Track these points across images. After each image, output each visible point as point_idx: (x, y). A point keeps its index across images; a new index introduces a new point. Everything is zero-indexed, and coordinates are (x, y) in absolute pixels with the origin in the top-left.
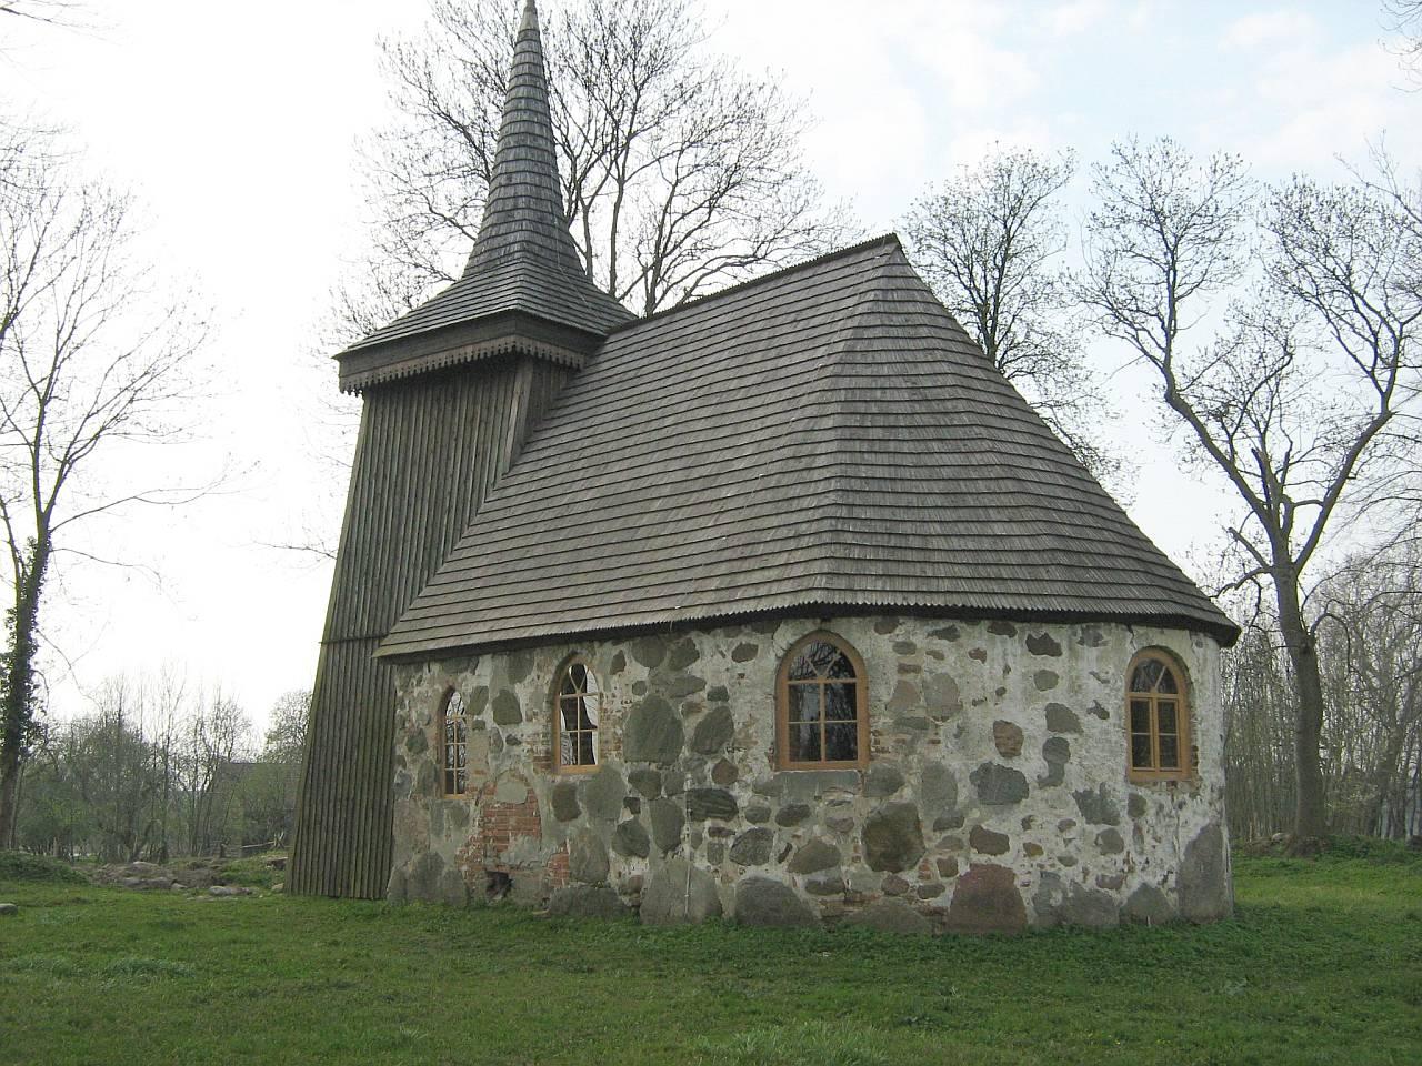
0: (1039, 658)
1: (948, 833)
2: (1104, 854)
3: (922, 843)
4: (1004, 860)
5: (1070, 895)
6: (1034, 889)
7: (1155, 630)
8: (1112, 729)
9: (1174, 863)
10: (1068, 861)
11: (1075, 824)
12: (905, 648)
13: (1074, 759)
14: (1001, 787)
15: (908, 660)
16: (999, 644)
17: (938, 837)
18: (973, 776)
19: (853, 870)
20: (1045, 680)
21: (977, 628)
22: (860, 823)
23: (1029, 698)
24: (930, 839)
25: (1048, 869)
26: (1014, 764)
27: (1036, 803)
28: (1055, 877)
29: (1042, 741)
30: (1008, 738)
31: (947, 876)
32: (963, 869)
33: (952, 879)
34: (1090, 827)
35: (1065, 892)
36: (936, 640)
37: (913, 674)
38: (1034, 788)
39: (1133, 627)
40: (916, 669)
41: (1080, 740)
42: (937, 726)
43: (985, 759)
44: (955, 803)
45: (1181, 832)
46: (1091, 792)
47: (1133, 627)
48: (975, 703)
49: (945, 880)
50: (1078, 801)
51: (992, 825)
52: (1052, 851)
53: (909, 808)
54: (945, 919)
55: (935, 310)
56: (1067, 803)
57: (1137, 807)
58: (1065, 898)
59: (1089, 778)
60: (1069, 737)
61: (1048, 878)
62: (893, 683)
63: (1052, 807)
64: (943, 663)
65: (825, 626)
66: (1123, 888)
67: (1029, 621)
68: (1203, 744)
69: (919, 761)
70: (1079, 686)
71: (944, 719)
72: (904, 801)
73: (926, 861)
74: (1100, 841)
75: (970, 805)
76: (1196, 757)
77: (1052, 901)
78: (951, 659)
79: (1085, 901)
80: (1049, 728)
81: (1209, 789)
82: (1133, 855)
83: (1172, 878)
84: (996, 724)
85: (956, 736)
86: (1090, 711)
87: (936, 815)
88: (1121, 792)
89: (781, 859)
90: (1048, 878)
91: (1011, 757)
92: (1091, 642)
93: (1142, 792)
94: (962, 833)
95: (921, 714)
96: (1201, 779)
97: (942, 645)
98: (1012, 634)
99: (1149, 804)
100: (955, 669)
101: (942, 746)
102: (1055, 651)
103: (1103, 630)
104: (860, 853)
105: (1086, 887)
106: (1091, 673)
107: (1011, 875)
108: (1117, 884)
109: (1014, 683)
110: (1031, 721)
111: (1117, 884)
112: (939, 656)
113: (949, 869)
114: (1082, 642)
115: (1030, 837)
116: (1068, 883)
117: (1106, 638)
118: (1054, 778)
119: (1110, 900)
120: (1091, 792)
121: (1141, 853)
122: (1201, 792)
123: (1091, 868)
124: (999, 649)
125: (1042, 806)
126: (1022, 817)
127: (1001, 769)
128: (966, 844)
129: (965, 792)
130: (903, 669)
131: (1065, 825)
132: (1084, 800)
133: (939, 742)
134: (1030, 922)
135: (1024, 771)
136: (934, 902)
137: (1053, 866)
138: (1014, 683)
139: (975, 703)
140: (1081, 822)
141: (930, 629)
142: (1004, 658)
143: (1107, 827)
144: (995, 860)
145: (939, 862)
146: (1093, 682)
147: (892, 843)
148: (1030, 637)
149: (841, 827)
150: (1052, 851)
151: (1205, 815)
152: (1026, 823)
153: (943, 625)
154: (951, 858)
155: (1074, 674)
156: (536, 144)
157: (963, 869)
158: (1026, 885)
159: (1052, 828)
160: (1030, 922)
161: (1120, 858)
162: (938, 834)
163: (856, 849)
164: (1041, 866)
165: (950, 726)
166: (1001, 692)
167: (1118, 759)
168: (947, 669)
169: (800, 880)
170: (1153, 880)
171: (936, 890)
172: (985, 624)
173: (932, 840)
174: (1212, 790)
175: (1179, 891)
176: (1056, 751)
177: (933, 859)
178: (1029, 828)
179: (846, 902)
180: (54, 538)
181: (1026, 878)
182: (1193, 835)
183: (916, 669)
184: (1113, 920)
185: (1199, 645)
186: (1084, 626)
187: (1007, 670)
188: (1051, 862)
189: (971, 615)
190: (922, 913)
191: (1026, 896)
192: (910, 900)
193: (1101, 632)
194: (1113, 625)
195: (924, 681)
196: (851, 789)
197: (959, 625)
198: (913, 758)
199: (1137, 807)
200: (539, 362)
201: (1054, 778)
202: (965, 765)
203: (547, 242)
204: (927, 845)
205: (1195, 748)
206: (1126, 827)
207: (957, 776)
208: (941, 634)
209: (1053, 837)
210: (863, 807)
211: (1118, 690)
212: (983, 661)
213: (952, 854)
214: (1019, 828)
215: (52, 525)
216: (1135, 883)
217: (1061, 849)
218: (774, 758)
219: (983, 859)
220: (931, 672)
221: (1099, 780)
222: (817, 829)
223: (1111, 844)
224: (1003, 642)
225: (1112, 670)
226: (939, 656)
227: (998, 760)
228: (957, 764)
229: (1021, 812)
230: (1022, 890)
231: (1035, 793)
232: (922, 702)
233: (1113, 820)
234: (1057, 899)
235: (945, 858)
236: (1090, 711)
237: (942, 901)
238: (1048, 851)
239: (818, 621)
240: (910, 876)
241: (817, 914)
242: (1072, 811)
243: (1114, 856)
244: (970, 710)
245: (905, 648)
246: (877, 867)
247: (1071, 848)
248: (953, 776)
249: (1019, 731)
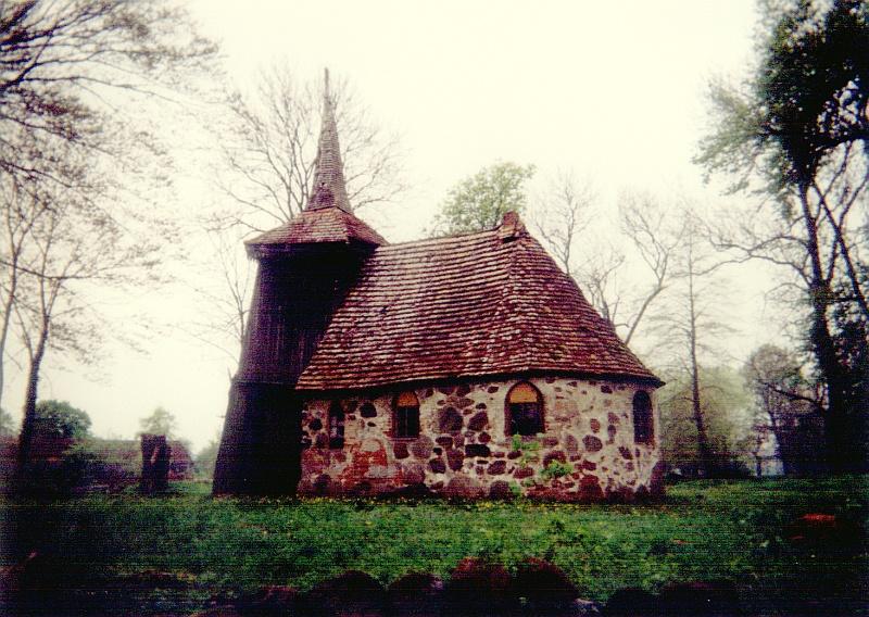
14: (593, 444)
26: (597, 435)
30: (595, 426)
32: (582, 476)
97: (571, 388)
107: (597, 479)
111: (633, 483)
129: (581, 446)
136: (571, 490)
157: (582, 476)
191: (603, 488)
198: (562, 433)
201: (611, 441)
217: (615, 469)
227: (592, 434)
228: (579, 437)
231: (604, 446)
234: (613, 489)
237: (574, 489)
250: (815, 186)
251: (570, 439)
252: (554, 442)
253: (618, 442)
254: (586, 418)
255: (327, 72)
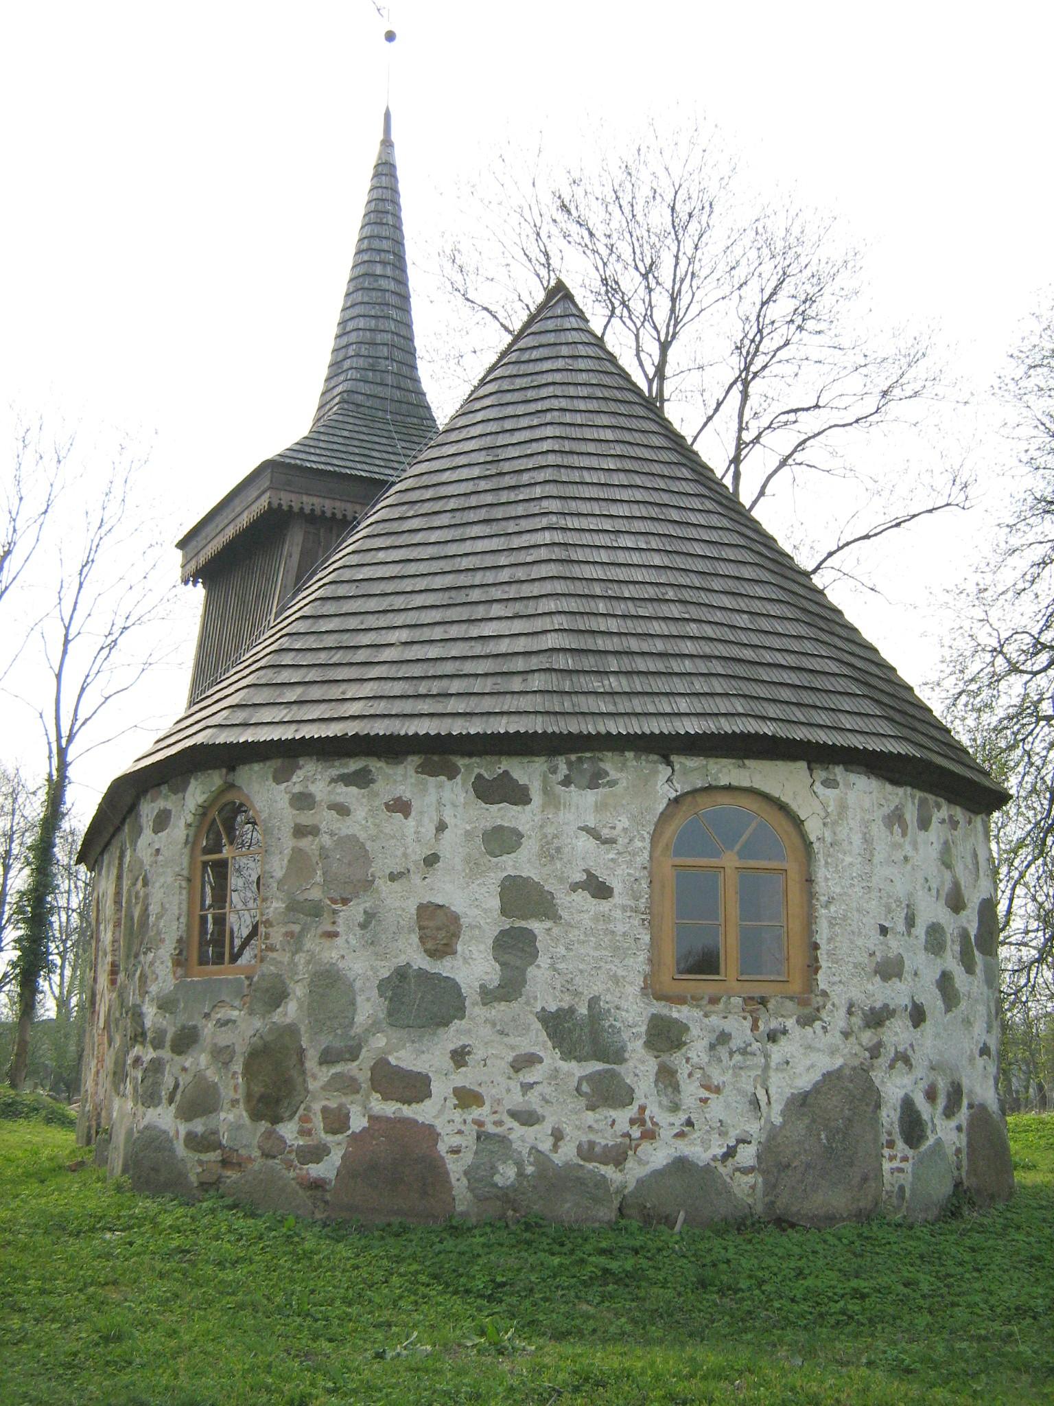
0: (495, 807)
1: (338, 1068)
2: (592, 1107)
3: (305, 1081)
4: (423, 1112)
5: (530, 1169)
6: (468, 1158)
7: (724, 761)
8: (618, 914)
9: (754, 1128)
10: (527, 1118)
11: (541, 1060)
12: (303, 801)
13: (543, 960)
14: (423, 1001)
15: (306, 818)
16: (432, 790)
17: (325, 1074)
18: (383, 985)
19: (231, 1119)
20: (501, 841)
21: (400, 770)
22: (241, 1049)
23: (474, 869)
24: (314, 1077)
25: (490, 1128)
26: (445, 968)
27: (475, 1026)
28: (503, 1140)
29: (492, 932)
30: (439, 930)
31: (334, 1133)
32: (358, 1122)
33: (339, 1137)
34: (565, 1066)
35: (519, 1165)
36: (341, 788)
37: (310, 838)
38: (474, 1004)
39: (674, 758)
40: (313, 831)
41: (556, 931)
42: (335, 912)
43: (402, 960)
44: (352, 1023)
45: (775, 1080)
46: (572, 1010)
47: (674, 758)
48: (393, 877)
49: (330, 1139)
50: (546, 1028)
51: (405, 1058)
52: (499, 1102)
53: (291, 1030)
54: (328, 1197)
55: (610, 367)
56: (527, 1028)
57: (665, 1036)
58: (521, 1174)
59: (569, 988)
60: (536, 926)
61: (490, 1142)
62: (288, 852)
63: (501, 1033)
64: (348, 821)
65: (230, 778)
66: (630, 1164)
67: (480, 754)
68: (830, 940)
69: (308, 962)
70: (558, 850)
71: (345, 901)
72: (288, 1021)
73: (308, 1109)
74: (585, 1088)
75: (374, 1027)
76: (817, 960)
77: (497, 1178)
78: (360, 813)
79: (552, 1180)
80: (504, 912)
81: (843, 1011)
82: (653, 1110)
83: (747, 1155)
84: (422, 908)
85: (363, 926)
86: (575, 887)
87: (325, 1041)
88: (632, 1013)
89: (171, 1101)
90: (490, 1142)
91: (441, 957)
92: (585, 782)
93: (679, 1013)
94: (359, 1069)
95: (315, 894)
96: (825, 994)
97: (349, 794)
98: (452, 773)
99: (695, 1031)
100: (366, 828)
101: (339, 941)
102: (520, 796)
103: (610, 764)
104: (240, 1095)
105: (558, 1159)
106: (585, 829)
107: (431, 1133)
108: (617, 1157)
109: (451, 846)
110: (476, 902)
111: (617, 1157)
112: (342, 810)
113: (337, 1121)
114: (567, 782)
115: (465, 1078)
116: (525, 1152)
117: (613, 774)
118: (509, 988)
119: (603, 1181)
120: (572, 1010)
121: (675, 1108)
122: (823, 1014)
123: (568, 1129)
124: (431, 798)
125: (486, 1031)
126: (452, 1047)
127: (422, 973)
128: (365, 1086)
129: (368, 1008)
130: (300, 831)
131: (526, 1061)
132: (559, 1027)
133: (335, 935)
134: (460, 1208)
135: (460, 978)
136: (316, 1170)
137: (499, 1123)
138: (451, 846)
139: (393, 877)
140: (551, 1058)
141: (334, 772)
142: (438, 810)
143: (598, 1066)
144: (407, 1111)
145: (325, 1110)
146: (585, 843)
147: (273, 1082)
148: (479, 776)
149: (222, 1055)
150: (499, 1102)
151: (833, 1052)
152: (460, 1057)
153: (354, 765)
154: (341, 1107)
155: (550, 830)
156: (375, 285)
157: (358, 1122)
158: (456, 1151)
159: (503, 1065)
160: (460, 1208)
161: (622, 1116)
162: (324, 1069)
163: (236, 1088)
164: (480, 1124)
165: (355, 911)
166: (431, 860)
167: (630, 961)
168: (356, 830)
169: (183, 1129)
170: (702, 1151)
171: (317, 1153)
172: (414, 761)
173: (318, 1077)
174: (850, 1013)
175: (764, 1172)
176: (515, 947)
177: (317, 1107)
178: (465, 1064)
179: (225, 1163)
180: (71, 772)
181: (456, 1141)
182: (805, 1082)
183: (313, 831)
184: (607, 1213)
185: (830, 783)
186: (573, 757)
187: (441, 827)
188: (496, 1117)
189: (392, 748)
190: (301, 1184)
191: (455, 1168)
192: (289, 1166)
193: (607, 766)
194: (630, 755)
195: (322, 848)
196: (237, 1003)
197: (375, 765)
198: (301, 958)
199: (665, 1036)
200: (313, 519)
201: (509, 988)
202: (372, 968)
203: (379, 390)
204: (311, 1087)
205: (816, 947)
206: (640, 1068)
207: (358, 985)
208: (347, 780)
209: (500, 1079)
210: (243, 1027)
211: (634, 854)
212: (406, 816)
213: (344, 1099)
214: (448, 1064)
215: (69, 759)
216: (658, 1156)
217: (516, 1099)
218: (179, 961)
219: (390, 1109)
220: (332, 834)
221: (588, 994)
222: (204, 1059)
223: (606, 1092)
224: (440, 786)
225: (623, 822)
226: (342, 810)
227: (420, 961)
228: (362, 966)
229: (451, 1037)
230: (449, 1158)
231: (476, 1011)
232: (319, 878)
233: (618, 1056)
234: (507, 1174)
235: (333, 1104)
236: (575, 887)
237: (326, 1169)
238: (494, 1102)
239: (224, 771)
240: (288, 1131)
241: (193, 1178)
242: (536, 1040)
243: (613, 1113)
244: (383, 885)
245: (303, 801)
246: (256, 1116)
247: (533, 1098)
248: (351, 986)
249: (455, 918)
250: (56, 998)
251: (329, 983)
252: (277, 996)
253: (544, 988)
254: (399, 903)
255: (387, 116)
